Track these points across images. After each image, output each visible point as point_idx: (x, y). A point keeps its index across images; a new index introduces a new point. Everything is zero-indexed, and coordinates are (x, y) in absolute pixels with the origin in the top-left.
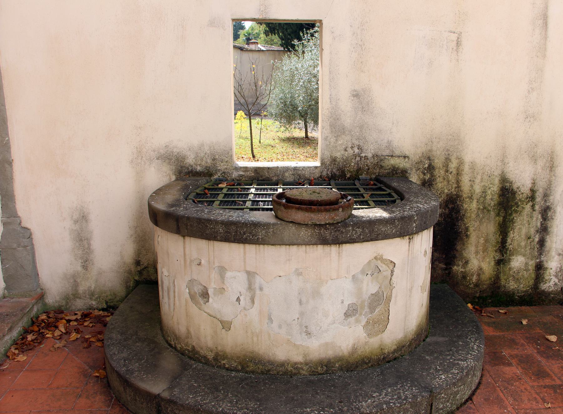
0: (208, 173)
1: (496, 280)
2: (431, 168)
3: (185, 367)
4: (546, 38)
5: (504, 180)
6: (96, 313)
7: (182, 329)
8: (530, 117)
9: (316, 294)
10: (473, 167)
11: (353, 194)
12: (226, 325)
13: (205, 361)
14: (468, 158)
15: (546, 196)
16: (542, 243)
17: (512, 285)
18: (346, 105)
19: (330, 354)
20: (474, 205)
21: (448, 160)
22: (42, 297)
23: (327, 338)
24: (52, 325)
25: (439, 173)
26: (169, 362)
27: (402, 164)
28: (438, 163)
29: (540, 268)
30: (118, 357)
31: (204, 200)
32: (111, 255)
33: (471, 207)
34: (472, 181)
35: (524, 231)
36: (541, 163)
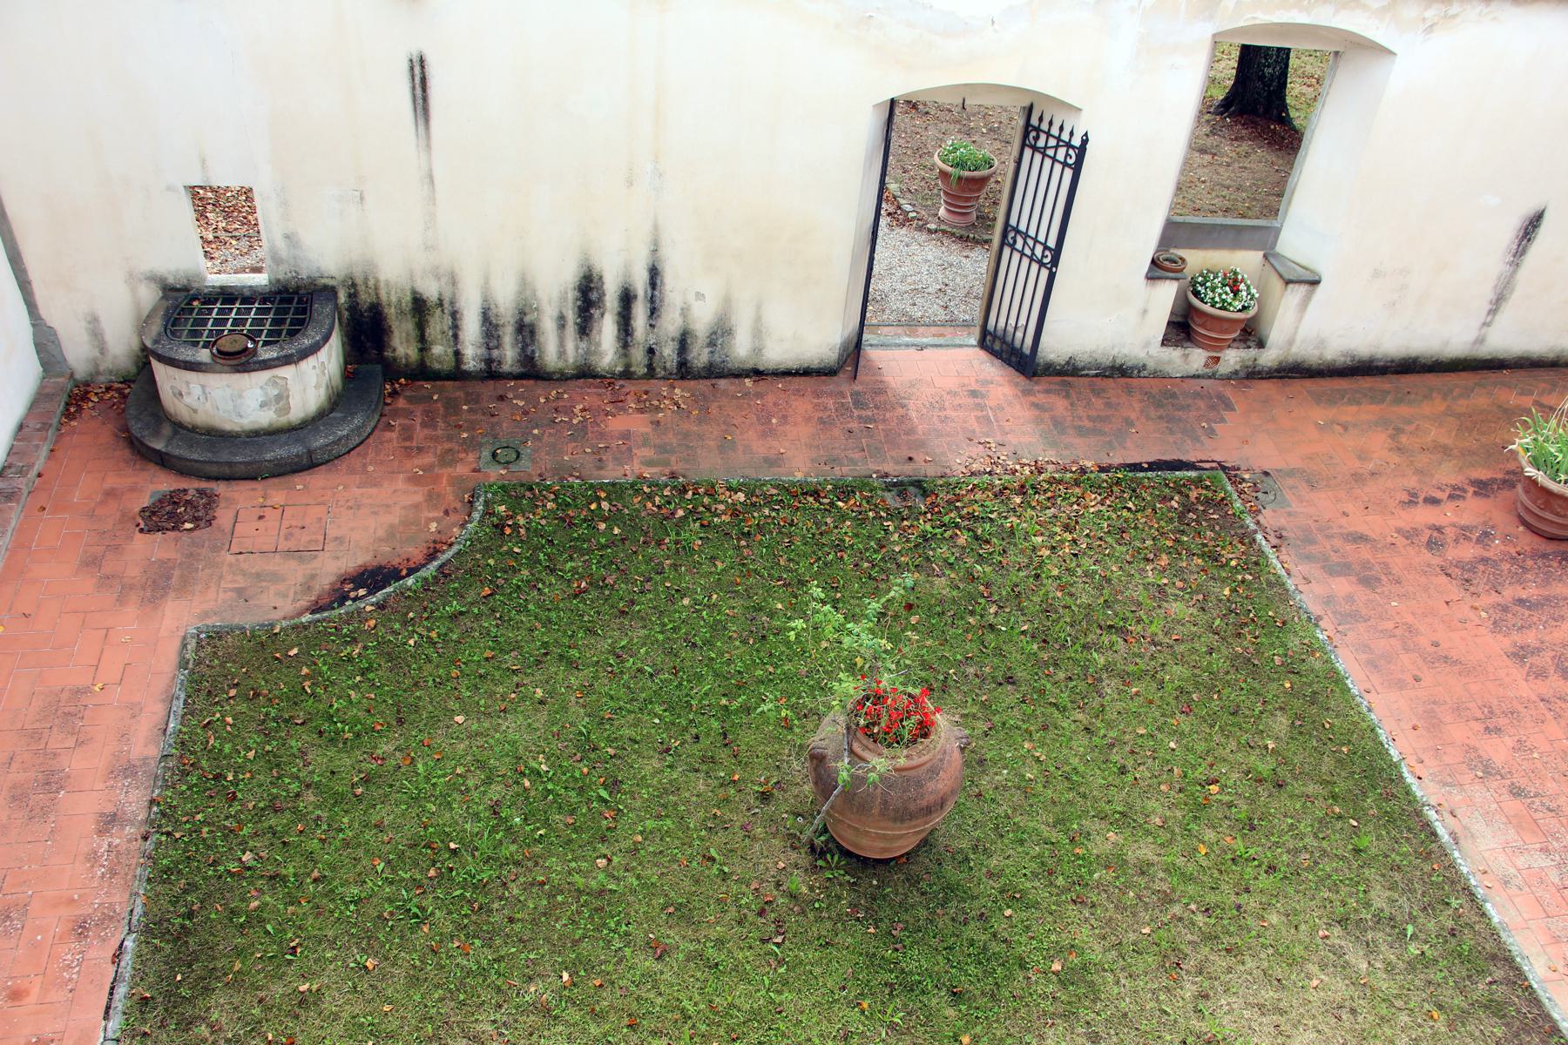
0: (186, 289)
1: (422, 363)
2: (354, 285)
3: (176, 433)
4: (434, 191)
5: (414, 292)
6: (117, 385)
7: (172, 411)
8: (429, 247)
9: (240, 396)
10: (387, 283)
11: (292, 308)
12: (195, 411)
13: (185, 428)
14: (382, 278)
15: (452, 303)
16: (456, 336)
17: (437, 366)
18: (281, 244)
19: (256, 426)
20: (393, 310)
21: (366, 279)
22: (72, 375)
23: (252, 418)
24: (85, 397)
25: (361, 288)
26: (167, 430)
27: (331, 283)
28: (359, 281)
29: (457, 354)
30: (136, 428)
31: (185, 310)
32: (121, 343)
33: (391, 312)
34: (388, 294)
35: (438, 328)
36: (444, 280)
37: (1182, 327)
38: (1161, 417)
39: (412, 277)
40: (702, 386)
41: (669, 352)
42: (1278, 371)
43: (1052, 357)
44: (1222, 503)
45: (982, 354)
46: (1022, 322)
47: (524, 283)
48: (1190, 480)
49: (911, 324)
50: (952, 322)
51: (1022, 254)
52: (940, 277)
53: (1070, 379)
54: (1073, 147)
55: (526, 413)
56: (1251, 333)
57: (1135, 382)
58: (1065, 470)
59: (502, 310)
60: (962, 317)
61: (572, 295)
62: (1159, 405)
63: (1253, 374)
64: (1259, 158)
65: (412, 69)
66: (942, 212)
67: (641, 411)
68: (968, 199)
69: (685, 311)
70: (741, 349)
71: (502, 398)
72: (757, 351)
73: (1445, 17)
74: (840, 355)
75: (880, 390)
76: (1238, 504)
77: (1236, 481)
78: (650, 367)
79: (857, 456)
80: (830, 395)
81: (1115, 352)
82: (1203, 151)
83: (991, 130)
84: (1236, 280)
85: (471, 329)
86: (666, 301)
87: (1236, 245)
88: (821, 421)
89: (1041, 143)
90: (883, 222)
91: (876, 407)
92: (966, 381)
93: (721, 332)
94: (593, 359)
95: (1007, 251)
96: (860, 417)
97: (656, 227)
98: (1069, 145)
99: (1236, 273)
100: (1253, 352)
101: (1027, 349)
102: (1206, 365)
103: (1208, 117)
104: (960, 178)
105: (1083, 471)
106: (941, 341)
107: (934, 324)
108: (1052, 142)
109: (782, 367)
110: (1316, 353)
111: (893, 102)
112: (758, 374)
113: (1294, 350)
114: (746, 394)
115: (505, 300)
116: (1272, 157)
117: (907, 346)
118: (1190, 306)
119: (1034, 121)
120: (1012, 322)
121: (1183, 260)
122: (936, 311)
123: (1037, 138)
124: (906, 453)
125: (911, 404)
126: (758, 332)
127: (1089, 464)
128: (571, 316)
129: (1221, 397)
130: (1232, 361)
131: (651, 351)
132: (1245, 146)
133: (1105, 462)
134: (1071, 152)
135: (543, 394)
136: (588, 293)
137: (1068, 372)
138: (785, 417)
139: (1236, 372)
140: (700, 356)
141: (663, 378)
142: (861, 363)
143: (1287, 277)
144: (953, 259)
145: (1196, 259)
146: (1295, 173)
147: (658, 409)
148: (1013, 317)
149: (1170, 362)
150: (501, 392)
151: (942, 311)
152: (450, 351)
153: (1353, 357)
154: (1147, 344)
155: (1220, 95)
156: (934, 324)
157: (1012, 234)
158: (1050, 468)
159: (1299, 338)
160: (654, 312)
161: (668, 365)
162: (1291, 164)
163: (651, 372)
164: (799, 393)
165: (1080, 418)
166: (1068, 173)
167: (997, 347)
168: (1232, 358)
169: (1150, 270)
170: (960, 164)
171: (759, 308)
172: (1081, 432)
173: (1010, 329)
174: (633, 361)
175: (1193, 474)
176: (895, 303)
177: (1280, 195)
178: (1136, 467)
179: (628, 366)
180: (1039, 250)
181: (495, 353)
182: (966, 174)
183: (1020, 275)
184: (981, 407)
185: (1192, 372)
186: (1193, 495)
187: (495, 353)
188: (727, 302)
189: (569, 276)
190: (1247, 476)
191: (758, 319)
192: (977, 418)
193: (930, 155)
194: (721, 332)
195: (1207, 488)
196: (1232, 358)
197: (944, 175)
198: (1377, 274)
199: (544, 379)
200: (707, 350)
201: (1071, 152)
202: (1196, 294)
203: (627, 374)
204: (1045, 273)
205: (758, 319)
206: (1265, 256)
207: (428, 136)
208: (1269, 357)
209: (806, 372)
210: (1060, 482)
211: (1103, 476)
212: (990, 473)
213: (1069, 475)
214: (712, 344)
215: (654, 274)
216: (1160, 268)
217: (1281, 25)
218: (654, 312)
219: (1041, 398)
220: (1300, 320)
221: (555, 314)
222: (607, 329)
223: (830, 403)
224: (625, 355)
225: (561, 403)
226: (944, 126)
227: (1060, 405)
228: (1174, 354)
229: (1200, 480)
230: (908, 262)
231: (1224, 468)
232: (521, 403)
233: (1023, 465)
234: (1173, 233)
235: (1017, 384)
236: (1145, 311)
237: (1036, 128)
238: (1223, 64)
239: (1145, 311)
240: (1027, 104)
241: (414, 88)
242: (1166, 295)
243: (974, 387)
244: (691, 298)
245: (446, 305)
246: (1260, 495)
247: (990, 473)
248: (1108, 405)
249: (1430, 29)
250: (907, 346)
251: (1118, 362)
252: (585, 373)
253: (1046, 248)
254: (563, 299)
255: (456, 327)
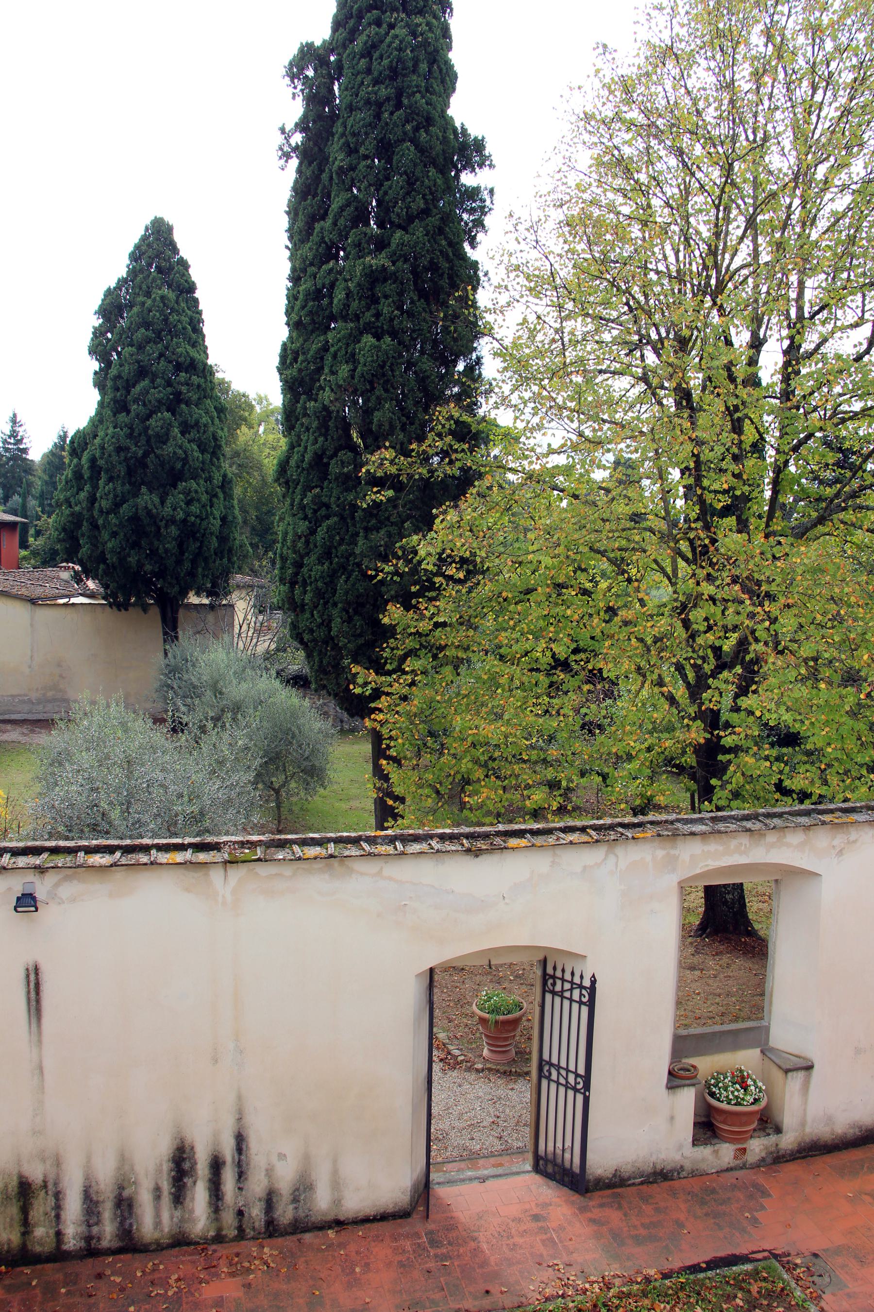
1: (24, 1247)
5: (21, 1177)
8: (36, 1132)
15: (56, 1184)
16: (58, 1217)
17: (38, 1249)
29: (59, 1234)
35: (41, 1210)
36: (48, 1163)
37: (707, 1126)
38: (707, 1215)
39: (19, 1162)
40: (289, 1242)
41: (256, 1212)
42: (799, 1151)
43: (599, 1172)
44: (783, 1294)
45: (538, 1178)
46: (568, 1143)
47: (123, 1159)
48: (747, 1273)
49: (472, 1158)
50: (507, 1151)
51: (558, 1083)
52: (491, 1110)
53: (619, 1190)
54: (585, 988)
55: (122, 1290)
56: (767, 1122)
57: (676, 1184)
58: (632, 1282)
59: (102, 1186)
60: (517, 1144)
61: (166, 1166)
62: (703, 1203)
63: (778, 1159)
64: (739, 966)
65: (28, 976)
66: (486, 1052)
67: (232, 1274)
68: (506, 1039)
69: (269, 1172)
70: (322, 1202)
71: (99, 1276)
72: (337, 1202)
73: (849, 842)
74: (412, 1197)
75: (451, 1225)
76: (798, 1293)
77: (790, 1268)
78: (240, 1229)
79: (437, 1296)
80: (407, 1236)
81: (654, 1159)
82: (692, 968)
83: (517, 977)
84: (743, 1077)
85: (73, 1207)
86: (252, 1166)
87: (736, 1046)
88: (401, 1264)
89: (558, 988)
90: (436, 1067)
91: (450, 1243)
92: (527, 1207)
93: (303, 1188)
94: (187, 1227)
95: (544, 1083)
96: (436, 1256)
97: (239, 1098)
98: (581, 987)
99: (741, 1071)
100: (773, 1138)
101: (576, 1168)
102: (735, 1158)
103: (690, 940)
104: (496, 1022)
105: (648, 1280)
106: (500, 1171)
107: (492, 1155)
108: (567, 986)
109: (361, 1215)
110: (827, 1129)
111: (432, 970)
112: (339, 1224)
113: (808, 1130)
114: (330, 1246)
115: (105, 1176)
116: (748, 964)
117: (471, 1179)
118: (710, 1107)
119: (550, 971)
120: (559, 1145)
121: (694, 1067)
122: (493, 1143)
123: (554, 984)
124: (483, 1287)
125: (481, 1237)
126: (336, 1184)
127: (652, 1272)
128: (166, 1187)
129: (756, 1186)
130: (757, 1150)
131: (240, 1213)
132: (725, 959)
133: (667, 1267)
134: (584, 992)
135: (140, 1266)
136: (181, 1163)
137: (616, 1183)
138: (367, 1265)
139: (763, 1159)
140: (285, 1213)
141: (253, 1238)
142: (432, 1202)
143: (785, 1067)
144: (500, 1092)
145: (706, 1064)
146: (769, 978)
147: (248, 1271)
148: (559, 1140)
149: (703, 1160)
150: (99, 1270)
151: (496, 1141)
152: (52, 1232)
153: (860, 1127)
154: (680, 1147)
155: (695, 921)
156: (492, 1155)
157: (546, 1068)
158: (617, 1282)
159: (809, 1119)
160: (241, 1175)
161: (257, 1224)
162: (765, 967)
163: (241, 1234)
164: (378, 1239)
165: (635, 1227)
166: (585, 1010)
167: (550, 1169)
168: (757, 1147)
169: (669, 1080)
170: (495, 1010)
171: (335, 1161)
172: (638, 1240)
173: (559, 1152)
174: (225, 1224)
175: (748, 1267)
176: (455, 1139)
177: (762, 994)
178: (695, 1269)
179: (219, 1229)
180: (571, 1078)
181: (95, 1230)
182: (501, 1017)
183: (559, 1102)
184: (544, 1230)
185: (725, 1165)
186: (754, 1289)
187: (95, 1230)
188: (307, 1159)
189: (165, 1148)
190: (798, 1261)
191: (335, 1173)
192: (543, 1241)
193: (470, 1004)
194: (303, 1188)
195: (765, 1279)
196: (757, 1147)
197: (483, 1021)
198: (858, 1051)
199: (141, 1251)
200: (291, 1207)
201: (584, 992)
202: (712, 1094)
203: (219, 1238)
204: (580, 1098)
205: (335, 1173)
206: (762, 1051)
207: (40, 1033)
208: (788, 1140)
209: (383, 1217)
210: (629, 1295)
211: (667, 1282)
212: (563, 1296)
213: (635, 1287)
214: (295, 1200)
215: (240, 1140)
216: (677, 1078)
217: (730, 866)
218: (241, 1175)
219: (597, 1213)
220: (805, 1102)
221: (152, 1186)
222: (199, 1196)
223: (408, 1245)
224: (217, 1220)
225: (157, 1275)
226: (478, 978)
227: (614, 1216)
228: (705, 1152)
229: (757, 1272)
230: (462, 1101)
231: (776, 1256)
232: (118, 1280)
233: (592, 1283)
234: (682, 1045)
235: (573, 1203)
236: (672, 1118)
237: (551, 975)
238: (693, 896)
239: (672, 1118)
240: (541, 957)
241: (29, 992)
242: (687, 1098)
243: (536, 1211)
244: (274, 1159)
245: (50, 1186)
246: (815, 1278)
247: (563, 1296)
248: (657, 1210)
249: (841, 853)
250: (471, 1179)
251: (659, 1167)
252: (180, 1241)
253: (577, 1075)
254: (159, 1171)
255: (58, 1207)
